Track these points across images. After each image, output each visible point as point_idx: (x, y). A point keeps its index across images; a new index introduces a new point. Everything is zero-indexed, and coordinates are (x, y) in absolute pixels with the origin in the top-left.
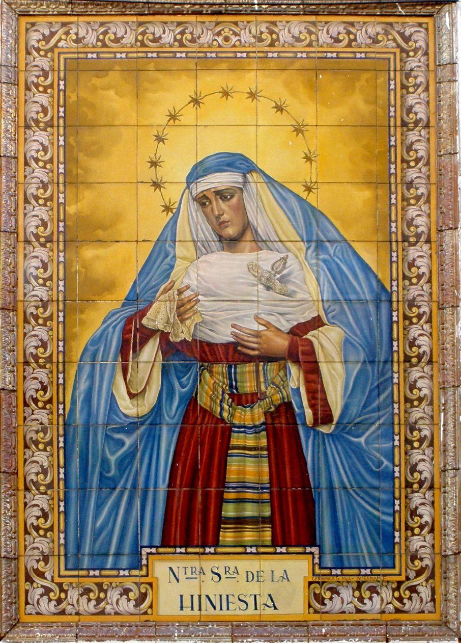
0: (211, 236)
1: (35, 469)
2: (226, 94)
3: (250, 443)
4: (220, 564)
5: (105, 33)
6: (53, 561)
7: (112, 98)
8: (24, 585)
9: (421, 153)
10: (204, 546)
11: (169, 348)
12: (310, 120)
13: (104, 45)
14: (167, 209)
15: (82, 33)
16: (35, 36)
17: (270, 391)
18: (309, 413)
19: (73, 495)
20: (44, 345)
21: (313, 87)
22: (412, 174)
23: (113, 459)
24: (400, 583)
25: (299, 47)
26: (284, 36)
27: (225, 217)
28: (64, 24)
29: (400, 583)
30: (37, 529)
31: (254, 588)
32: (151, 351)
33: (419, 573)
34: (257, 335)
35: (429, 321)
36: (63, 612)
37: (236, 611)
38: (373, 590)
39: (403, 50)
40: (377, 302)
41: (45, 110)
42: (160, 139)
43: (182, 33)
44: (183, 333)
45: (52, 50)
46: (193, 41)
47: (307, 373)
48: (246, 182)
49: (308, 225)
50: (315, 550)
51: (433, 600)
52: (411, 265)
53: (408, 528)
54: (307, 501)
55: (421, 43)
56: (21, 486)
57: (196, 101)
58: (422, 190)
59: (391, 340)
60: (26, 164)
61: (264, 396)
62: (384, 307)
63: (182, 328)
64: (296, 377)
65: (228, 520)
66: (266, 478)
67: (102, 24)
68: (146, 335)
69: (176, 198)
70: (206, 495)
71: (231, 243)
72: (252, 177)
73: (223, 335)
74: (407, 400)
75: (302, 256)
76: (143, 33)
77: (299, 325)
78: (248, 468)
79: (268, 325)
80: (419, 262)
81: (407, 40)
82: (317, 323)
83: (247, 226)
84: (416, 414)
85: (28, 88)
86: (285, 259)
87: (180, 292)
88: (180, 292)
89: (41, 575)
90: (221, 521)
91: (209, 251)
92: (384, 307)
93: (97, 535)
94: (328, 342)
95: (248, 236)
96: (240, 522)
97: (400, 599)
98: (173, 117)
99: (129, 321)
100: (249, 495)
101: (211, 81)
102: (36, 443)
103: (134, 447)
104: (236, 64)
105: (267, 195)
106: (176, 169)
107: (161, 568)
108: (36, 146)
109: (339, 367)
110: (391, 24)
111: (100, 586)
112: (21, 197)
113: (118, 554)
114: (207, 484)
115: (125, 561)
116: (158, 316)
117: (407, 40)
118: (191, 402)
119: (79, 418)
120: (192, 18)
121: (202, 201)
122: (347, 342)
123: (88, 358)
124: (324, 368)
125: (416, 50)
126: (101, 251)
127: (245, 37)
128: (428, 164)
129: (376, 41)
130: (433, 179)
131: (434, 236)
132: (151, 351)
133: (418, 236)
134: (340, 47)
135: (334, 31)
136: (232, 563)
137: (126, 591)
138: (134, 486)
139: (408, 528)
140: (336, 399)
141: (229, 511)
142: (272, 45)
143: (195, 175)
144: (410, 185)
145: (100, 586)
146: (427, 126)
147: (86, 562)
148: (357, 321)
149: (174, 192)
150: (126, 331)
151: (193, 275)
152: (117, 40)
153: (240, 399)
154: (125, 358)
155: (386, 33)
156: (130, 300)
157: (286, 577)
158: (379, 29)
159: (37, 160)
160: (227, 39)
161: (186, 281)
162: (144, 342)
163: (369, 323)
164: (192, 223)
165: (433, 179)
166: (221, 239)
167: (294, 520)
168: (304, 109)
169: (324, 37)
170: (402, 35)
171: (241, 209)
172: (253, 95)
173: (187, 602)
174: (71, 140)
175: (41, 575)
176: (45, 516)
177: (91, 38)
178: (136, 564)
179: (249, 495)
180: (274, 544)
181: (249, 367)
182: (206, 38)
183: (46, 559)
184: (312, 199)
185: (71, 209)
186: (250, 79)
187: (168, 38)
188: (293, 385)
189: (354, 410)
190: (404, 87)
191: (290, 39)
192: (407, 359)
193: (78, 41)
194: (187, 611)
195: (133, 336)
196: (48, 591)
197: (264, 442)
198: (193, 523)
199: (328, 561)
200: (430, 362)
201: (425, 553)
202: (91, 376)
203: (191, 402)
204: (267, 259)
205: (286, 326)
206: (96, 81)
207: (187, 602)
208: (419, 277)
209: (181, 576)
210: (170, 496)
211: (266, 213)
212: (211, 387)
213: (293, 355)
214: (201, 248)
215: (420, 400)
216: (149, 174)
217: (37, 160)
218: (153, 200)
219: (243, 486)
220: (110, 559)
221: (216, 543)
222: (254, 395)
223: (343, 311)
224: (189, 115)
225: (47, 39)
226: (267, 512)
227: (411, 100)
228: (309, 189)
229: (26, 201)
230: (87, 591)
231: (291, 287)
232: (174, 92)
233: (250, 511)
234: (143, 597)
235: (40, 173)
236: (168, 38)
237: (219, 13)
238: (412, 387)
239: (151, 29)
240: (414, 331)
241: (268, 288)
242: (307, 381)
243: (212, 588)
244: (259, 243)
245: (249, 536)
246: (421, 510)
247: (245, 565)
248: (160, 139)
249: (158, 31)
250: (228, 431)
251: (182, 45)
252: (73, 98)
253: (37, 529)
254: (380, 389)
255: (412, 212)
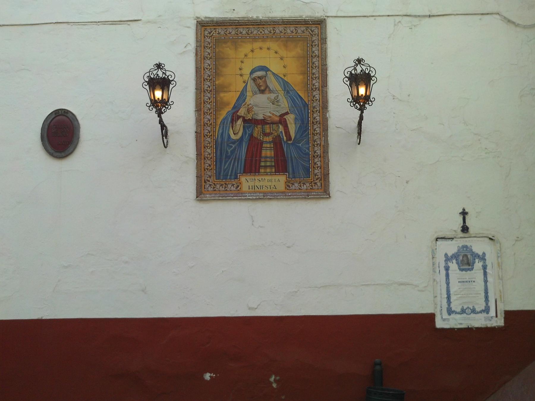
0: (257, 89)
1: (207, 153)
2: (261, 48)
3: (268, 146)
4: (260, 178)
5: (226, 31)
6: (212, 177)
7: (228, 51)
8: (203, 184)
9: (317, 65)
10: (255, 173)
11: (245, 121)
12: (285, 56)
13: (226, 35)
14: (244, 82)
15: (220, 31)
16: (206, 32)
17: (274, 132)
18: (285, 138)
19: (218, 160)
20: (209, 120)
21: (286, 46)
22: (314, 71)
23: (229, 151)
24: (312, 182)
25: (282, 34)
26: (278, 31)
27: (261, 84)
28: (215, 29)
29: (312, 182)
30: (208, 169)
31: (270, 183)
32: (240, 122)
33: (317, 179)
34: (270, 117)
35: (319, 112)
36: (215, 190)
37: (265, 189)
38: (304, 184)
39: (311, 35)
40: (304, 106)
41: (209, 54)
42: (242, 62)
43: (248, 31)
44: (249, 117)
45: (211, 36)
46: (251, 33)
47: (284, 127)
48: (267, 73)
49: (284, 86)
50: (287, 174)
51: (321, 186)
52: (314, 97)
53: (314, 167)
54: (285, 162)
55: (317, 32)
56: (203, 158)
57: (252, 51)
58: (317, 75)
59: (308, 117)
60: (204, 70)
61: (272, 134)
62: (306, 108)
63: (249, 115)
64: (281, 128)
65: (262, 166)
66: (273, 155)
67: (225, 29)
68: (239, 117)
69: (247, 79)
70: (256, 160)
71: (262, 92)
72: (269, 73)
73: (260, 117)
74: (313, 134)
75: (283, 95)
76: (237, 31)
77: (282, 114)
78: (268, 152)
79: (273, 114)
80: (316, 96)
81: (312, 31)
82: (287, 113)
83: (267, 87)
84: (316, 137)
85: (204, 48)
86: (278, 96)
87: (248, 106)
88: (248, 106)
89: (209, 181)
90: (260, 167)
91: (256, 94)
92: (306, 108)
93: (224, 171)
94: (290, 119)
95: (267, 89)
96: (266, 167)
97: (312, 186)
98: (246, 55)
99: (234, 113)
100: (268, 160)
101: (257, 45)
102: (207, 147)
103: (235, 148)
104: (264, 39)
105: (273, 78)
106: (247, 71)
107: (243, 179)
108: (207, 64)
109: (294, 125)
110: (308, 27)
111: (226, 184)
112: (203, 79)
113: (231, 175)
114: (256, 157)
115: (233, 177)
116: (242, 112)
117: (312, 31)
118: (251, 136)
119: (219, 140)
120: (251, 26)
121: (254, 80)
122: (296, 119)
123: (222, 124)
124: (289, 125)
125: (315, 35)
126: (225, 94)
127: (266, 32)
128: (319, 68)
129: (304, 32)
130: (320, 72)
131: (320, 89)
132: (240, 122)
133: (316, 88)
134: (293, 34)
135: (291, 29)
136: (263, 177)
137: (233, 185)
138: (235, 158)
139: (314, 167)
140: (293, 134)
141: (263, 164)
142: (274, 34)
143: (252, 73)
144: (313, 74)
145: (226, 184)
146: (318, 57)
147: (222, 178)
148: (298, 112)
149: (246, 78)
150: (233, 116)
151: (252, 101)
152: (230, 33)
153: (266, 134)
154: (233, 124)
155: (307, 30)
156: (234, 107)
157: (279, 180)
158: (305, 28)
159: (207, 69)
160: (261, 32)
161: (250, 102)
162: (238, 119)
163: (302, 113)
164: (251, 86)
165: (320, 72)
166: (259, 90)
167: (281, 166)
168: (283, 52)
169: (289, 31)
170: (311, 30)
171: (265, 82)
172: (268, 49)
173: (251, 187)
174: (217, 63)
175: (209, 181)
176: (210, 166)
177: (222, 33)
178: (236, 178)
179: (268, 160)
180: (275, 172)
181: (268, 126)
182: (255, 32)
183: (210, 177)
184: (285, 79)
185: (217, 83)
186: (269, 44)
187: (244, 32)
188: (280, 130)
189: (298, 137)
190: (311, 45)
191: (279, 32)
192: (313, 123)
193: (219, 33)
194: (251, 190)
195: (234, 117)
196: (210, 185)
197: (272, 146)
198: (252, 167)
199: (291, 176)
200: (320, 123)
201: (319, 174)
202: (223, 129)
203: (251, 136)
204: (272, 96)
205: (278, 114)
206: (224, 45)
207: (251, 187)
208: (316, 100)
209: (249, 180)
210: (245, 160)
211: (273, 83)
212: (257, 131)
213: (280, 122)
214: (254, 93)
215: (317, 134)
216: (239, 72)
217: (207, 69)
218: (240, 80)
219: (266, 157)
220: (229, 177)
221: (259, 172)
222: (269, 133)
223: (294, 110)
224: (250, 55)
225: (210, 33)
226: (273, 164)
227: (314, 49)
228: (285, 76)
229: (204, 80)
230: (222, 185)
231: (280, 104)
232: (246, 48)
233: (268, 164)
234: (238, 186)
235: (208, 72)
236: (244, 32)
237: (259, 25)
238: (315, 130)
239: (239, 30)
240: (315, 115)
241: (273, 104)
242: (285, 129)
243: (258, 184)
244: (271, 91)
245: (268, 170)
246: (317, 163)
247: (267, 178)
248: (242, 62)
249: (242, 30)
250: (262, 143)
251: (248, 34)
252: (217, 50)
253: (208, 169)
254: (305, 131)
255: (314, 82)
